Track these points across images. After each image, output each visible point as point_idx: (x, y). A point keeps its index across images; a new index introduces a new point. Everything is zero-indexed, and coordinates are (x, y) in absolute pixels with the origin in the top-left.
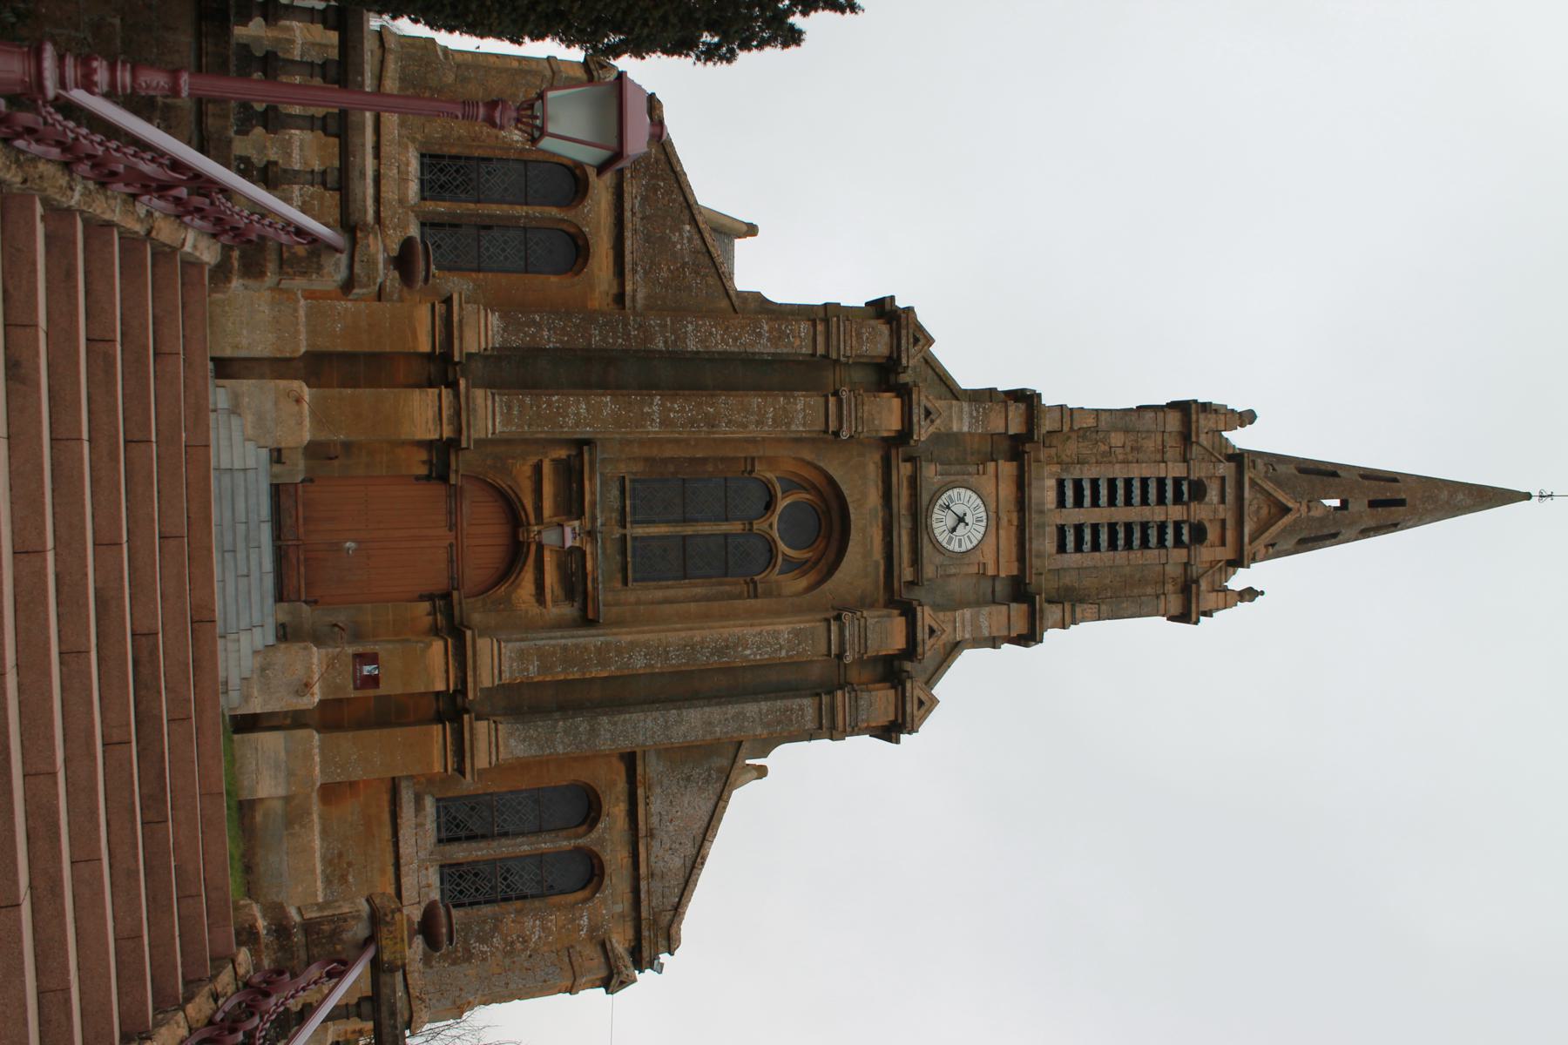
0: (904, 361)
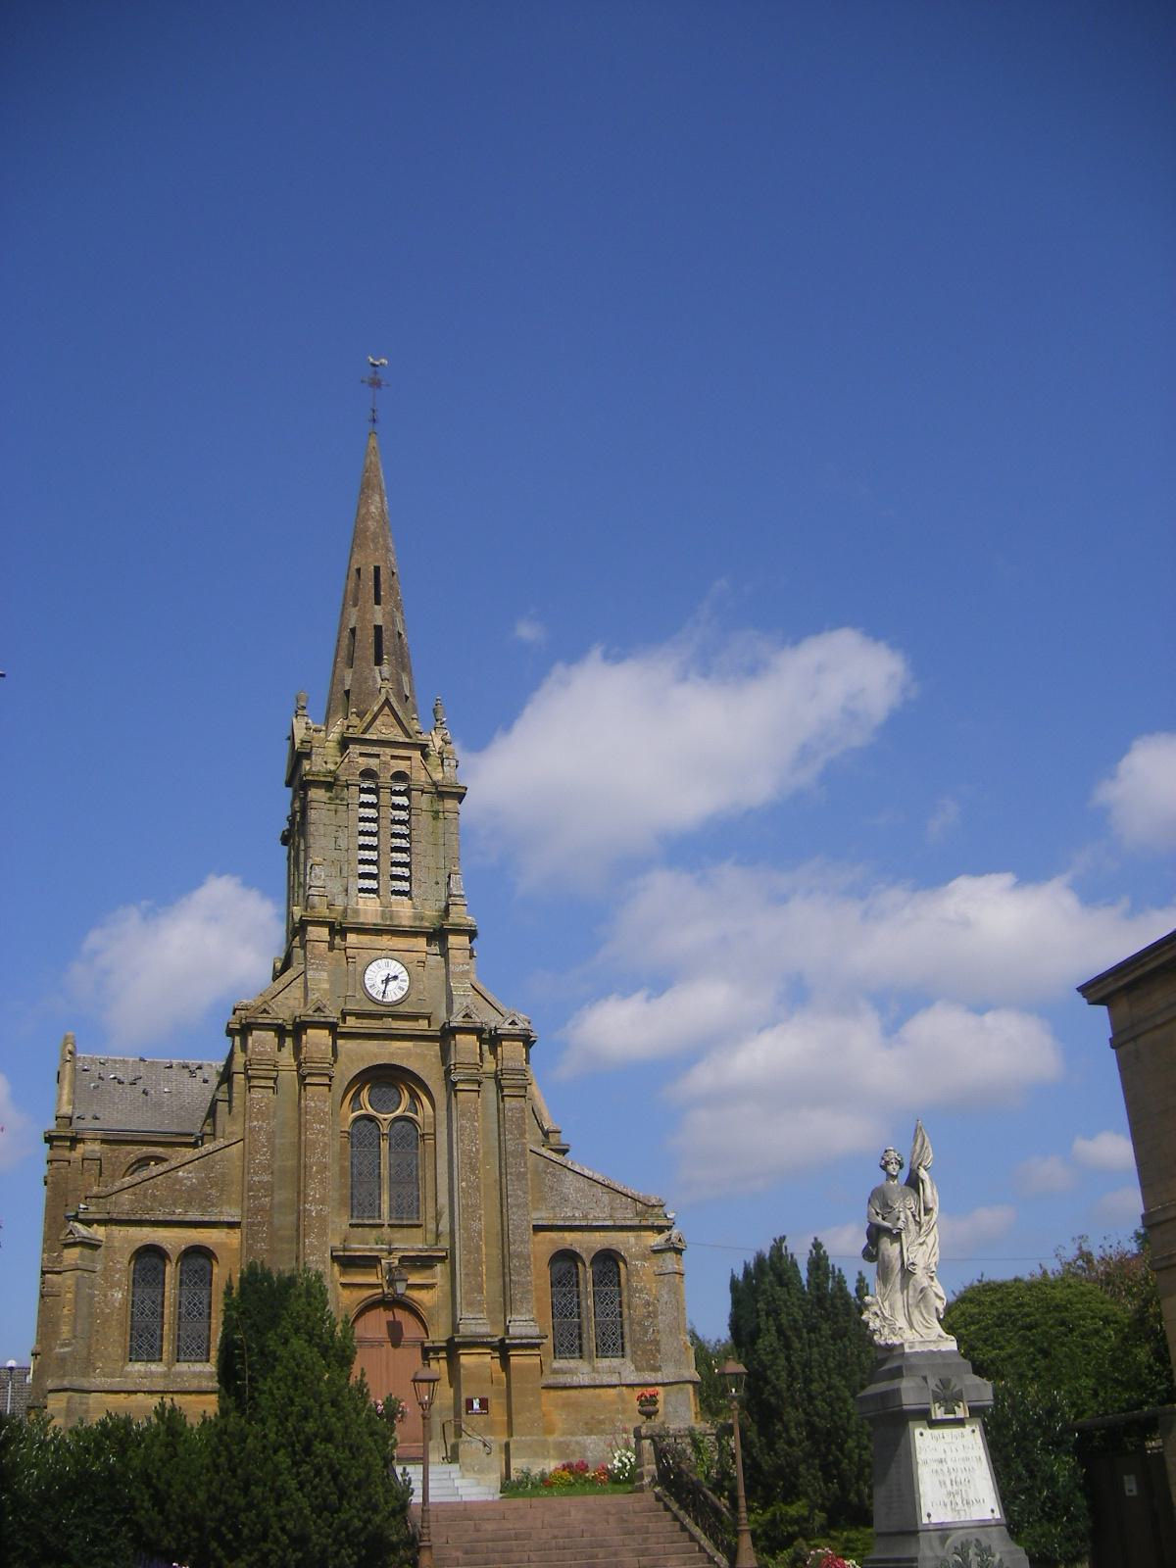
0: (280, 1021)
